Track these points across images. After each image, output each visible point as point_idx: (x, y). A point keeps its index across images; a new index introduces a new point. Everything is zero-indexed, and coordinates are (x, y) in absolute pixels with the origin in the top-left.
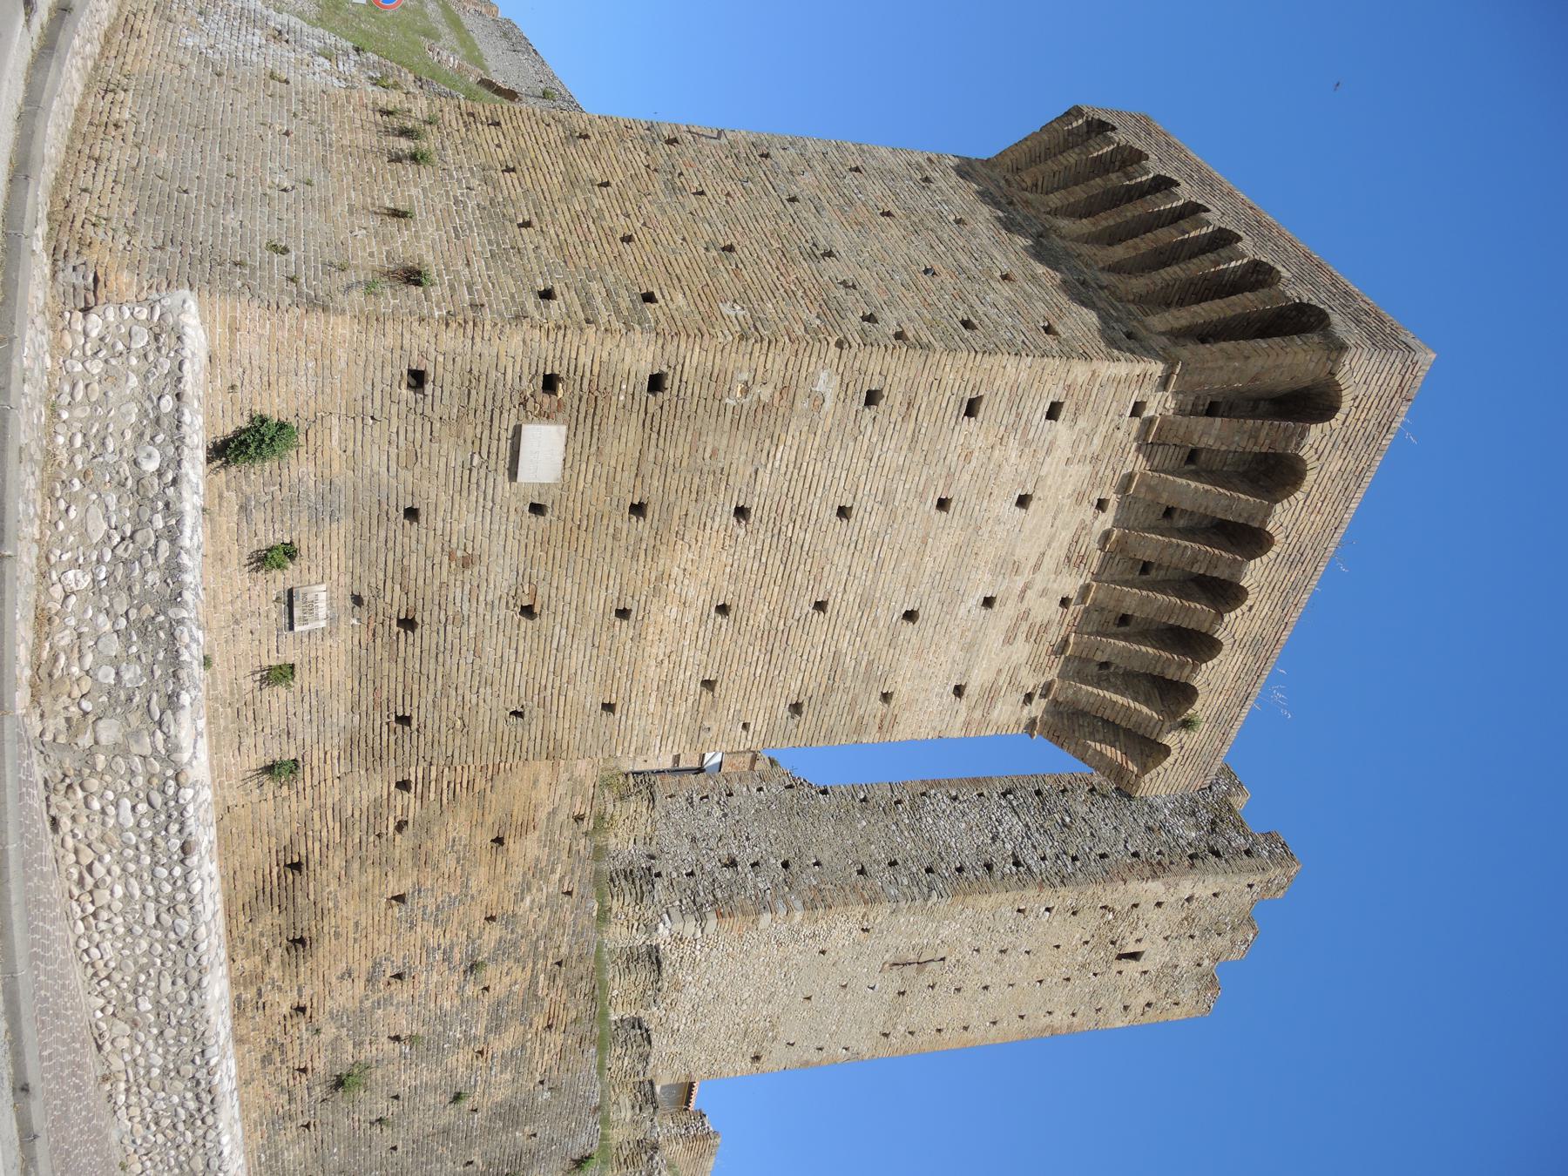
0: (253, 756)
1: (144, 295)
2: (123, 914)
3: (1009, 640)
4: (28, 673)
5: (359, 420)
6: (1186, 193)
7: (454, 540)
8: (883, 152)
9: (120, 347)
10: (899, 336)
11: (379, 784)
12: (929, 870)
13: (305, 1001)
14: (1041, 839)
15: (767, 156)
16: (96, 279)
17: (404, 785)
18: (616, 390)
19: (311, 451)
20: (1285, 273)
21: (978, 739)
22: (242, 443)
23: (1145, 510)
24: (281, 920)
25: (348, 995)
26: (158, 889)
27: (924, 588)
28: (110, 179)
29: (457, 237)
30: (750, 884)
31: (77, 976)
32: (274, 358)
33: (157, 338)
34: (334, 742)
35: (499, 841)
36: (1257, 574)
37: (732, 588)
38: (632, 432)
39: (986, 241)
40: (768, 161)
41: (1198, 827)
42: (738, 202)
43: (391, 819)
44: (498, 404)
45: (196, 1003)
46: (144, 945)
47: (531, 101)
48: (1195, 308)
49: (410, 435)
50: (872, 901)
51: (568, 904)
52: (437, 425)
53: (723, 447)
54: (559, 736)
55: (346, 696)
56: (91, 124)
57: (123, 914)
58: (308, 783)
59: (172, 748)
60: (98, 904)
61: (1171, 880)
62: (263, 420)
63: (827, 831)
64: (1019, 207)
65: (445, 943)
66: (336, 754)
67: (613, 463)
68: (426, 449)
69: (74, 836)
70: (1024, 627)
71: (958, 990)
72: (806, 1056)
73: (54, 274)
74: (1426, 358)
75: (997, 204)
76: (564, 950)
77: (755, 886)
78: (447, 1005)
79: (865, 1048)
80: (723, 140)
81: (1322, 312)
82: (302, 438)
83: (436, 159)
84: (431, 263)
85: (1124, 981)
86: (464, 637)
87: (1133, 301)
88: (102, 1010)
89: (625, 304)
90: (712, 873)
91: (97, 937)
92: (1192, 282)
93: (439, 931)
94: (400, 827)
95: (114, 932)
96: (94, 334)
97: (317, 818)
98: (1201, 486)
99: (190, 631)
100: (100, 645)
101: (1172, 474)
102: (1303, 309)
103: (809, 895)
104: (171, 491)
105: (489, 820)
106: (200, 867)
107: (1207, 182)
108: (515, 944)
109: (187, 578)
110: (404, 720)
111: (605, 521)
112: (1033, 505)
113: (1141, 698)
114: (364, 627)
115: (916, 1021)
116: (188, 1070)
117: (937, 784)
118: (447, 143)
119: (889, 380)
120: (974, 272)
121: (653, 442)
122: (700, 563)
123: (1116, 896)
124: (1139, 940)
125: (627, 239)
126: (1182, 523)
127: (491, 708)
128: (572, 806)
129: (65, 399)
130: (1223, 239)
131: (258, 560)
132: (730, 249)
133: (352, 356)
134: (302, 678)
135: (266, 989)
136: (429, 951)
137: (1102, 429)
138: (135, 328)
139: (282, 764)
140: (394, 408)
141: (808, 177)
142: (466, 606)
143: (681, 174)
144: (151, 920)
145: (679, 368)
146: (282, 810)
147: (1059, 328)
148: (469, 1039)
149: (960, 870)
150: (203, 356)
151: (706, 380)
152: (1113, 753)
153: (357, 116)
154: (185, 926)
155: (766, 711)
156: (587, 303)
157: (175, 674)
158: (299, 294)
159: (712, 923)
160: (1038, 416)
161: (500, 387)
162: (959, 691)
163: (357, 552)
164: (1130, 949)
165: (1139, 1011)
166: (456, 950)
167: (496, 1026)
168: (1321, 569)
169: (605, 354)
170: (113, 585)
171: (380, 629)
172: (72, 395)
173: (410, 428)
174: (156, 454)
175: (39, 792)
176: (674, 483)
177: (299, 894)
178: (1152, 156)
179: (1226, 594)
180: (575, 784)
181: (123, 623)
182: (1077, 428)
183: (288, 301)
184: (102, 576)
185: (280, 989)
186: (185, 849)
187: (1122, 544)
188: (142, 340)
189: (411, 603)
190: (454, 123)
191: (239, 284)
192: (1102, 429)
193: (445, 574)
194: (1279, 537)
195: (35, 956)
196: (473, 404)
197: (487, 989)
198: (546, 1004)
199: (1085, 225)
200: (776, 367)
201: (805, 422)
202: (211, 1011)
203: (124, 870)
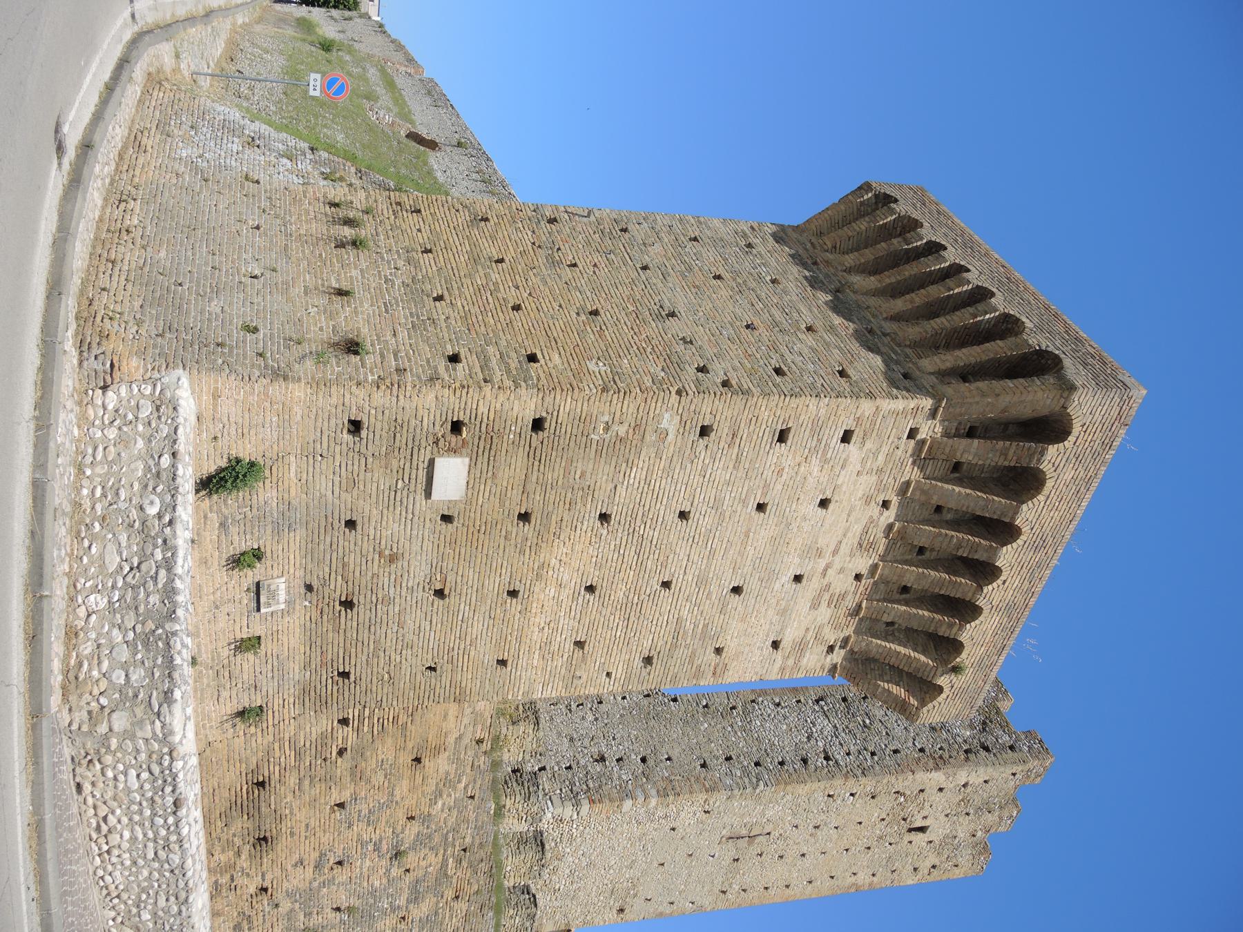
1: (149, 375)
2: (130, 851)
3: (815, 606)
4: (60, 678)
5: (311, 458)
6: (952, 256)
7: (383, 542)
8: (716, 223)
9: (130, 417)
10: (726, 384)
11: (325, 722)
12: (757, 764)
13: (267, 884)
14: (847, 738)
15: (624, 230)
16: (112, 365)
17: (344, 722)
18: (507, 431)
19: (275, 480)
20: (1028, 324)
22: (221, 479)
23: (919, 508)
24: (249, 824)
25: (300, 878)
26: (156, 834)
27: (747, 569)
28: (123, 278)
29: (387, 311)
30: (616, 776)
31: (95, 896)
32: (247, 416)
33: (158, 410)
34: (290, 692)
35: (418, 760)
36: (1009, 557)
37: (597, 573)
38: (519, 461)
39: (794, 298)
40: (627, 235)
42: (603, 272)
43: (334, 747)
44: (417, 443)
45: (184, 914)
46: (145, 873)
47: (448, 149)
48: (958, 353)
49: (350, 467)
50: (711, 790)
51: (471, 805)
52: (370, 460)
54: (463, 685)
55: (300, 658)
56: (108, 231)
57: (130, 851)
58: (270, 723)
59: (167, 733)
60: (111, 844)
61: (950, 771)
62: (238, 461)
63: (676, 732)
64: (822, 266)
65: (375, 837)
66: (292, 700)
67: (505, 484)
68: (361, 477)
69: (94, 796)
70: (826, 597)
71: (781, 857)
72: (661, 909)
73: (81, 363)
74: (1139, 393)
75: (804, 265)
76: (468, 840)
77: (620, 778)
78: (377, 884)
79: (707, 902)
80: (592, 218)
81: (1057, 356)
82: (267, 472)
83: (371, 244)
84: (366, 335)
85: (913, 848)
86: (391, 613)
87: (909, 346)
88: (114, 920)
89: (514, 364)
90: (585, 767)
91: (110, 868)
92: (955, 330)
93: (371, 828)
94: (341, 752)
95: (122, 864)
96: (110, 407)
97: (277, 748)
98: (963, 490)
99: (182, 640)
100: (114, 654)
101: (941, 481)
102: (1042, 354)
103: (662, 784)
104: (168, 530)
105: (410, 745)
106: (187, 816)
107: (969, 245)
108: (430, 837)
109: (180, 599)
110: (345, 675)
111: (499, 526)
112: (831, 506)
113: (920, 648)
114: (314, 608)
117: (764, 693)
118: (380, 229)
119: (718, 418)
120: (785, 325)
121: (536, 468)
122: (572, 555)
123: (906, 783)
124: (925, 817)
125: (516, 308)
126: (949, 516)
127: (412, 664)
128: (474, 732)
129: (89, 459)
130: (980, 295)
131: (234, 562)
132: (595, 313)
133: (306, 412)
134: (267, 646)
135: (237, 875)
136: (363, 844)
137: (885, 449)
138: (142, 402)
139: (251, 710)
140: (338, 448)
141: (657, 248)
142: (392, 591)
143: (559, 249)
144: (151, 855)
145: (555, 413)
146: (250, 744)
147: (850, 372)
148: (394, 909)
149: (782, 763)
150: (193, 419)
151: (577, 422)
152: (898, 691)
153: (311, 208)
154: (176, 859)
155: (623, 664)
156: (485, 366)
157: (170, 675)
158: (266, 367)
159: (585, 807)
160: (835, 440)
161: (418, 431)
162: (775, 645)
164: (918, 824)
165: (926, 872)
166: (384, 842)
167: (415, 898)
168: (1060, 551)
169: (498, 406)
170: (124, 605)
171: (326, 609)
172: (94, 456)
173: (350, 463)
174: (157, 501)
176: (552, 497)
177: (263, 804)
178: (925, 224)
179: (985, 572)
180: (477, 717)
181: (131, 635)
182: (865, 449)
183: (257, 373)
184: (116, 599)
185: (248, 875)
186: (177, 804)
187: (902, 534)
188: (147, 410)
189: (350, 590)
190: (385, 212)
191: (220, 361)
192: (885, 449)
193: (376, 567)
195: (65, 893)
196: (397, 444)
197: (408, 871)
198: (454, 881)
199: (872, 282)
200: (630, 410)
202: (195, 919)
203: (130, 820)
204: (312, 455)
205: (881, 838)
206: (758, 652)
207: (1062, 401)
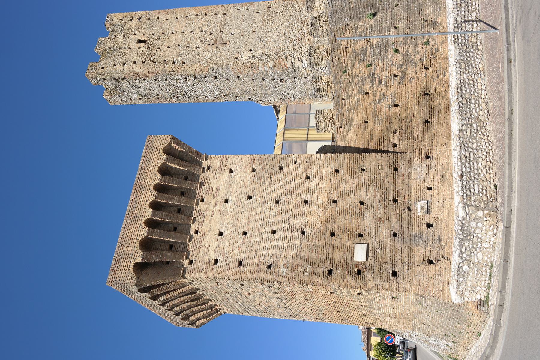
0: (439, 161)
12: (216, 77)
21: (223, 154)
26: (469, 164)
35: (366, 122)
38: (336, 258)
41: (122, 87)
45: (461, 125)
52: (389, 261)
53: (310, 253)
59: (464, 208)
70: (214, 192)
71: (202, 32)
77: (274, 74)
104: (461, 261)
110: (395, 169)
112: (218, 233)
115: (214, 19)
116: (464, 102)
122: (314, 217)
124: (140, 48)
137: (201, 256)
144: (472, 154)
147: (215, 283)
149: (206, 77)
154: (463, 152)
162: (231, 171)
163: (410, 224)
164: (142, 45)
175: (499, 197)
185: (432, 77)
186: (462, 176)
194: (143, 225)
201: (288, 260)
204: (410, 264)
205: (158, 38)
206: (238, 168)
207: (139, 280)
